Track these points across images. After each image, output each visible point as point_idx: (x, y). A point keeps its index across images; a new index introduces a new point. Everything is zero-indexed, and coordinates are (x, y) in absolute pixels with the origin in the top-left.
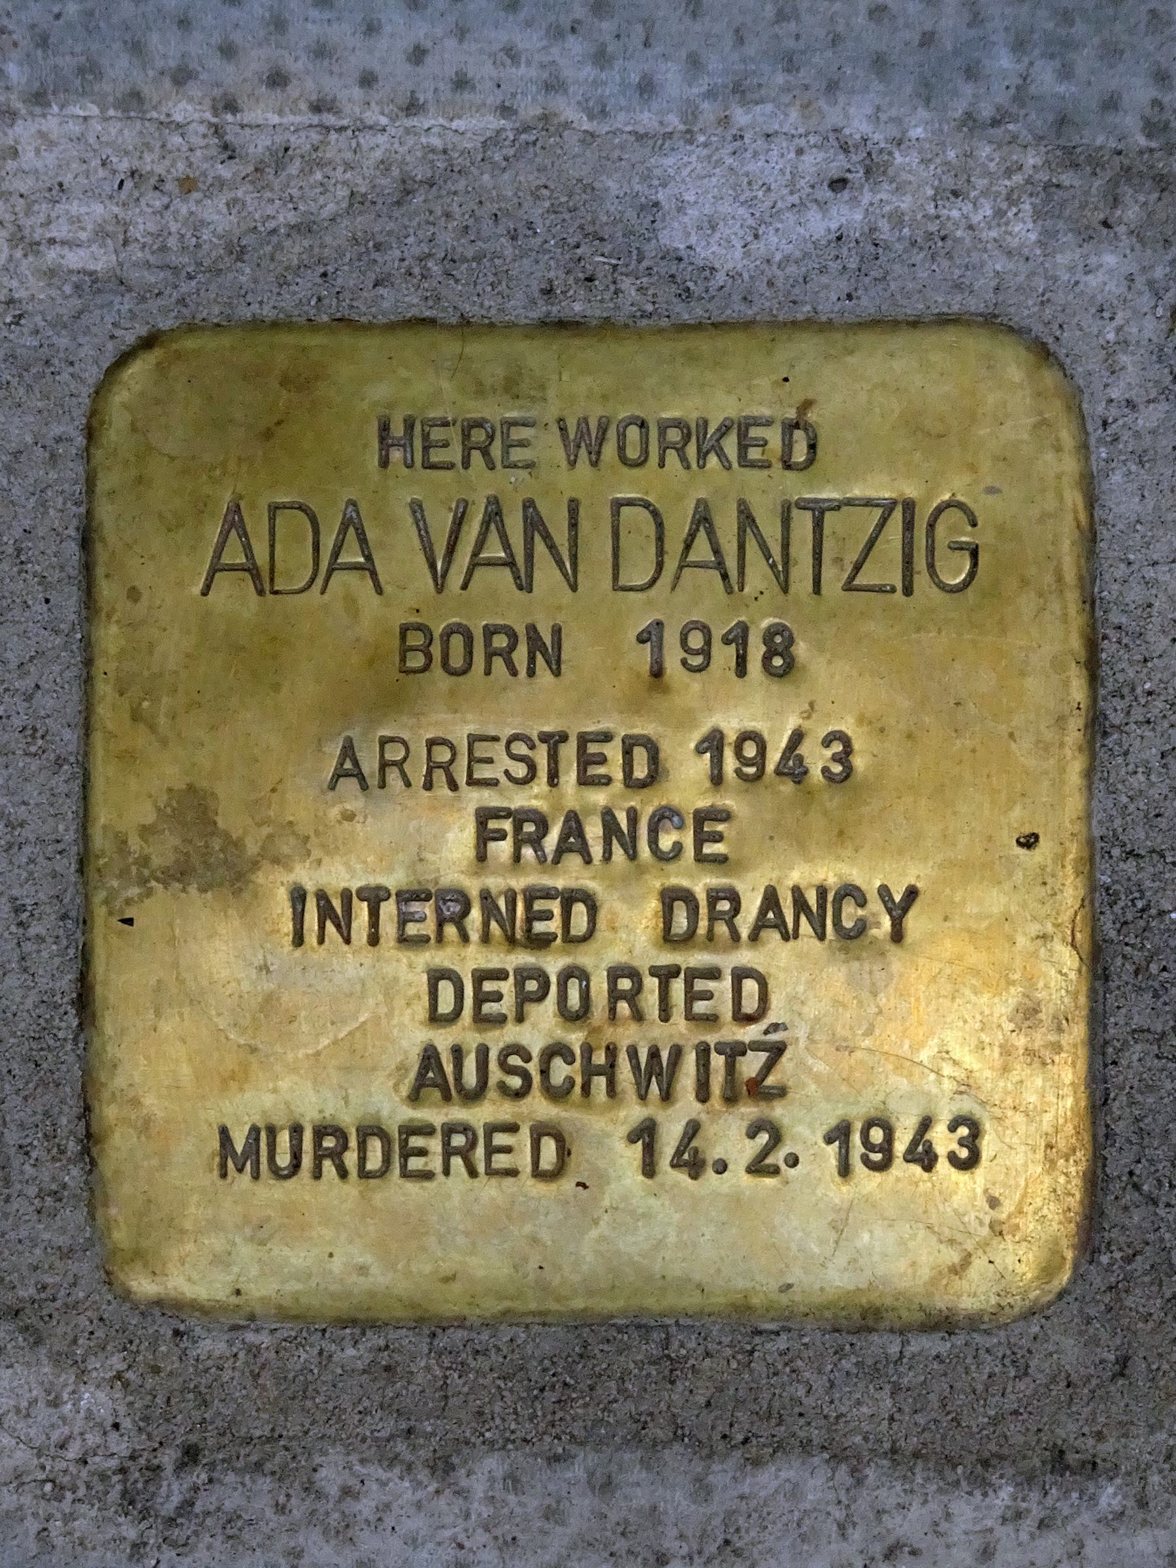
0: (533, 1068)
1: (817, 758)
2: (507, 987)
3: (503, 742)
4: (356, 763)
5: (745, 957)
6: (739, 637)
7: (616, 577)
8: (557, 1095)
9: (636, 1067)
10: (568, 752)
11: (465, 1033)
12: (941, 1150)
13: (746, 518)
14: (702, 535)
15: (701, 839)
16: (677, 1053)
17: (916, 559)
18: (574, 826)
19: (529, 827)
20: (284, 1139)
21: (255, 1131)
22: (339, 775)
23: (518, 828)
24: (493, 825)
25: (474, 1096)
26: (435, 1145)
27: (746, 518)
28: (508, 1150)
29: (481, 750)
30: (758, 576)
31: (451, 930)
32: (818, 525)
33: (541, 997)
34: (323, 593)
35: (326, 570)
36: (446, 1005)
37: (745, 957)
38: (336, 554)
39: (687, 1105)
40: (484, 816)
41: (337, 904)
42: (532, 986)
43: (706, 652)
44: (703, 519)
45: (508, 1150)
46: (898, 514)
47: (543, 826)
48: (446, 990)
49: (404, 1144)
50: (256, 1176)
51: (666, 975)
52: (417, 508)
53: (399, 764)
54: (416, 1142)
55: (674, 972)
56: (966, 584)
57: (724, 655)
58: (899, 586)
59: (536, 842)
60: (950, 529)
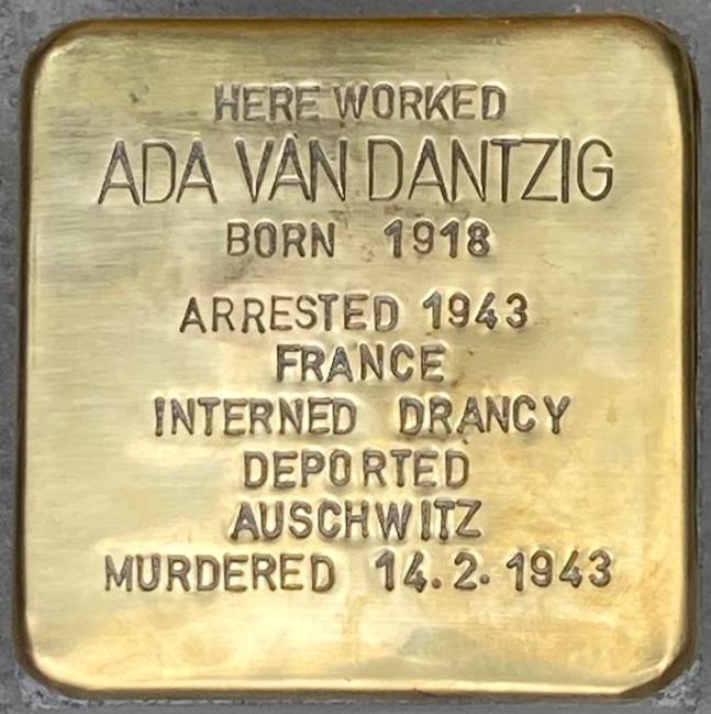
0: (314, 517)
1: (503, 312)
2: (297, 464)
3: (296, 300)
4: (198, 315)
5: (456, 446)
6: (452, 232)
7: (371, 194)
8: (328, 537)
9: (380, 516)
10: (338, 307)
11: (269, 497)
12: (585, 574)
13: (457, 152)
14: (428, 161)
15: (425, 366)
16: (408, 509)
17: (570, 179)
18: (341, 357)
19: (311, 359)
20: (147, 565)
21: (128, 560)
22: (185, 323)
23: (304, 358)
24: (288, 356)
25: (271, 538)
26: (247, 568)
27: (457, 152)
28: (296, 572)
29: (280, 306)
30: (466, 192)
31: (259, 426)
32: (506, 153)
33: (319, 470)
34: (178, 201)
35: (177, 190)
36: (255, 477)
37: (456, 446)
38: (186, 176)
39: (413, 541)
40: (281, 350)
41: (293, 409)
42: (312, 463)
43: (430, 241)
44: (429, 151)
45: (296, 572)
46: (559, 149)
47: (320, 356)
48: (256, 465)
49: (226, 567)
50: (129, 589)
51: (400, 457)
52: (241, 148)
53: (226, 316)
54: (234, 567)
55: (407, 454)
56: (465, 478)
57: (444, 243)
58: (559, 195)
59: (316, 367)
60: (596, 156)
